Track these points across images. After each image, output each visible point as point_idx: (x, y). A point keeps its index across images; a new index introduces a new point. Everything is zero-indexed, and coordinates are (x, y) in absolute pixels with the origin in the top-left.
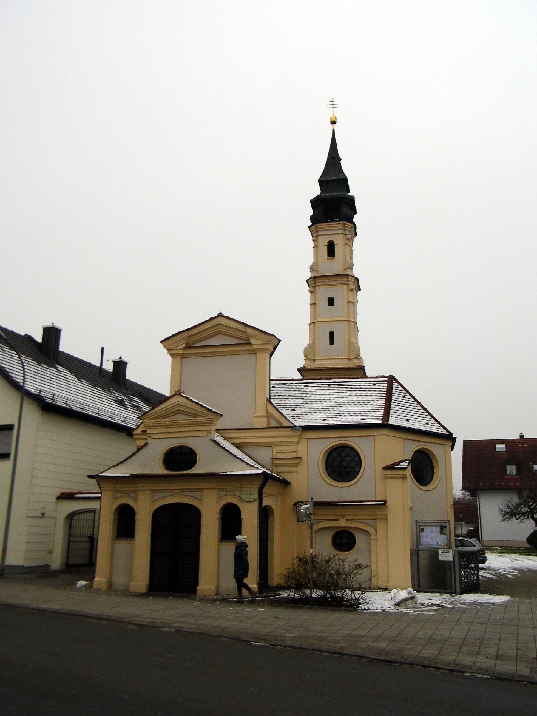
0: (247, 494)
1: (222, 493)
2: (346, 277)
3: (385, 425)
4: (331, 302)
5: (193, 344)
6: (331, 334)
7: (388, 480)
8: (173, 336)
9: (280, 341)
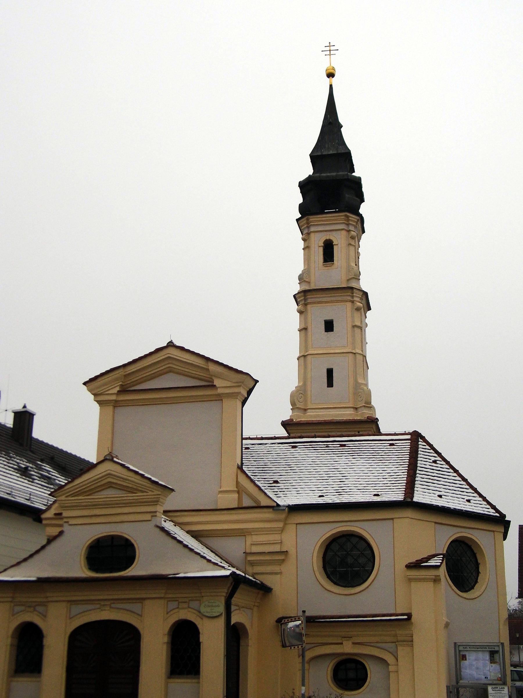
0: (209, 606)
1: (173, 605)
2: (350, 291)
4: (329, 326)
5: (131, 387)
6: (330, 373)
7: (413, 584)
8: (102, 375)
9: (257, 381)
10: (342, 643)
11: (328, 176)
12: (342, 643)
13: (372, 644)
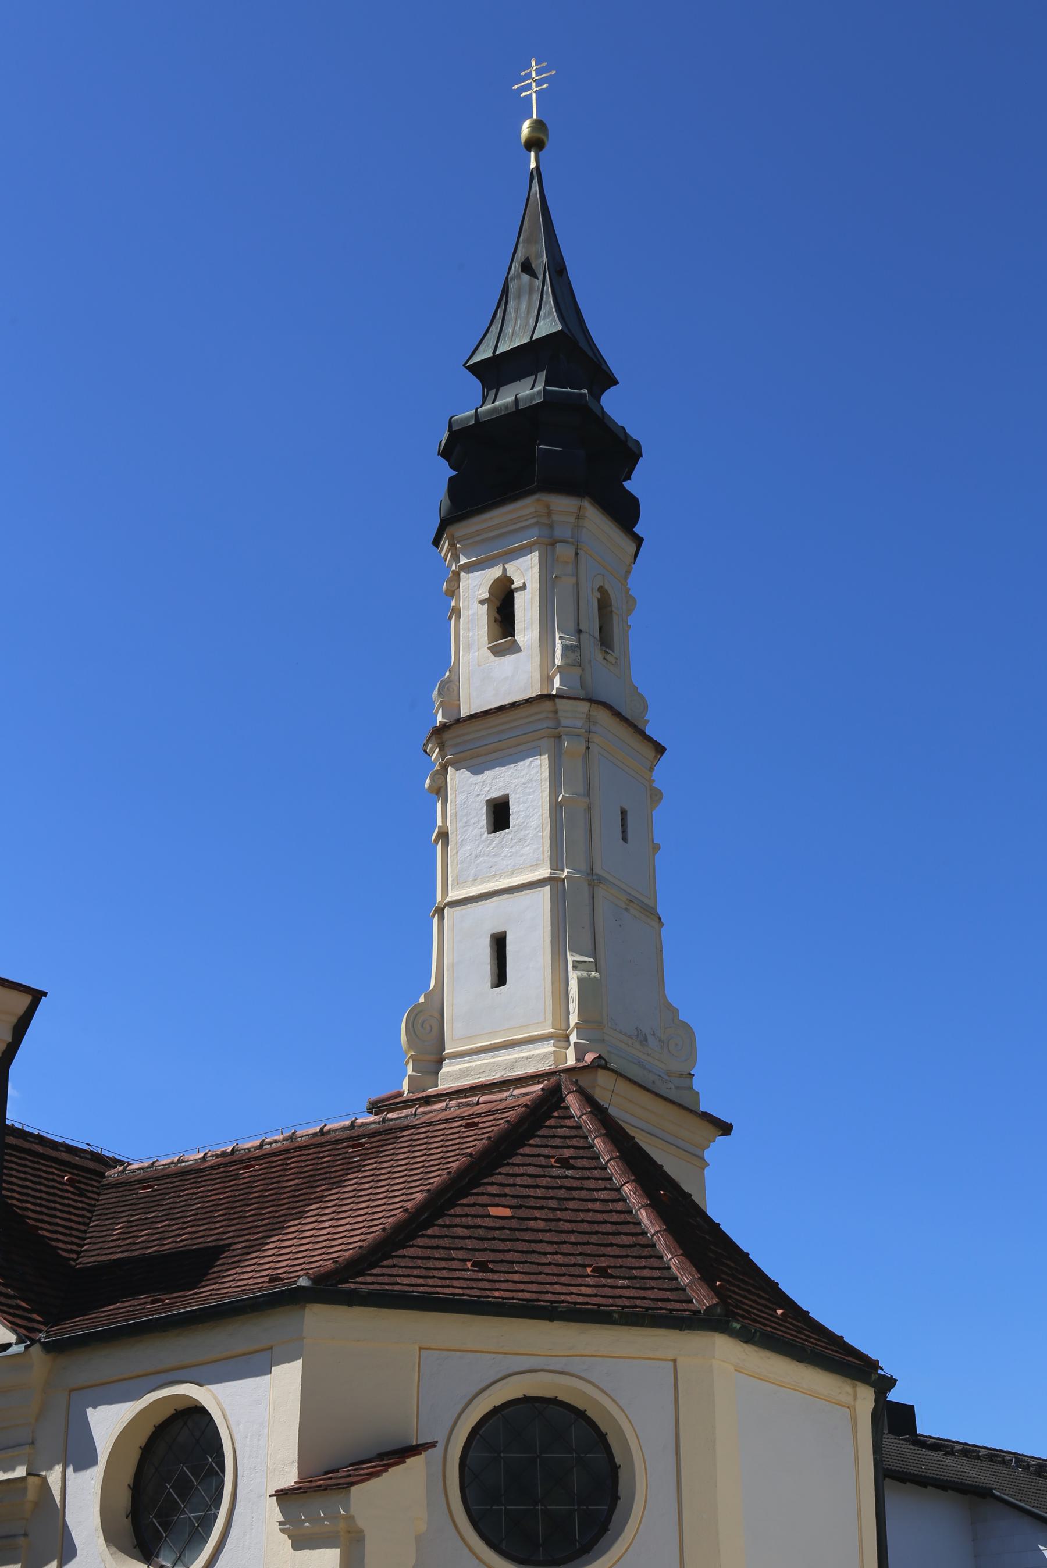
4: (499, 815)
6: (499, 943)
9: (37, 996)
11: (495, 410)
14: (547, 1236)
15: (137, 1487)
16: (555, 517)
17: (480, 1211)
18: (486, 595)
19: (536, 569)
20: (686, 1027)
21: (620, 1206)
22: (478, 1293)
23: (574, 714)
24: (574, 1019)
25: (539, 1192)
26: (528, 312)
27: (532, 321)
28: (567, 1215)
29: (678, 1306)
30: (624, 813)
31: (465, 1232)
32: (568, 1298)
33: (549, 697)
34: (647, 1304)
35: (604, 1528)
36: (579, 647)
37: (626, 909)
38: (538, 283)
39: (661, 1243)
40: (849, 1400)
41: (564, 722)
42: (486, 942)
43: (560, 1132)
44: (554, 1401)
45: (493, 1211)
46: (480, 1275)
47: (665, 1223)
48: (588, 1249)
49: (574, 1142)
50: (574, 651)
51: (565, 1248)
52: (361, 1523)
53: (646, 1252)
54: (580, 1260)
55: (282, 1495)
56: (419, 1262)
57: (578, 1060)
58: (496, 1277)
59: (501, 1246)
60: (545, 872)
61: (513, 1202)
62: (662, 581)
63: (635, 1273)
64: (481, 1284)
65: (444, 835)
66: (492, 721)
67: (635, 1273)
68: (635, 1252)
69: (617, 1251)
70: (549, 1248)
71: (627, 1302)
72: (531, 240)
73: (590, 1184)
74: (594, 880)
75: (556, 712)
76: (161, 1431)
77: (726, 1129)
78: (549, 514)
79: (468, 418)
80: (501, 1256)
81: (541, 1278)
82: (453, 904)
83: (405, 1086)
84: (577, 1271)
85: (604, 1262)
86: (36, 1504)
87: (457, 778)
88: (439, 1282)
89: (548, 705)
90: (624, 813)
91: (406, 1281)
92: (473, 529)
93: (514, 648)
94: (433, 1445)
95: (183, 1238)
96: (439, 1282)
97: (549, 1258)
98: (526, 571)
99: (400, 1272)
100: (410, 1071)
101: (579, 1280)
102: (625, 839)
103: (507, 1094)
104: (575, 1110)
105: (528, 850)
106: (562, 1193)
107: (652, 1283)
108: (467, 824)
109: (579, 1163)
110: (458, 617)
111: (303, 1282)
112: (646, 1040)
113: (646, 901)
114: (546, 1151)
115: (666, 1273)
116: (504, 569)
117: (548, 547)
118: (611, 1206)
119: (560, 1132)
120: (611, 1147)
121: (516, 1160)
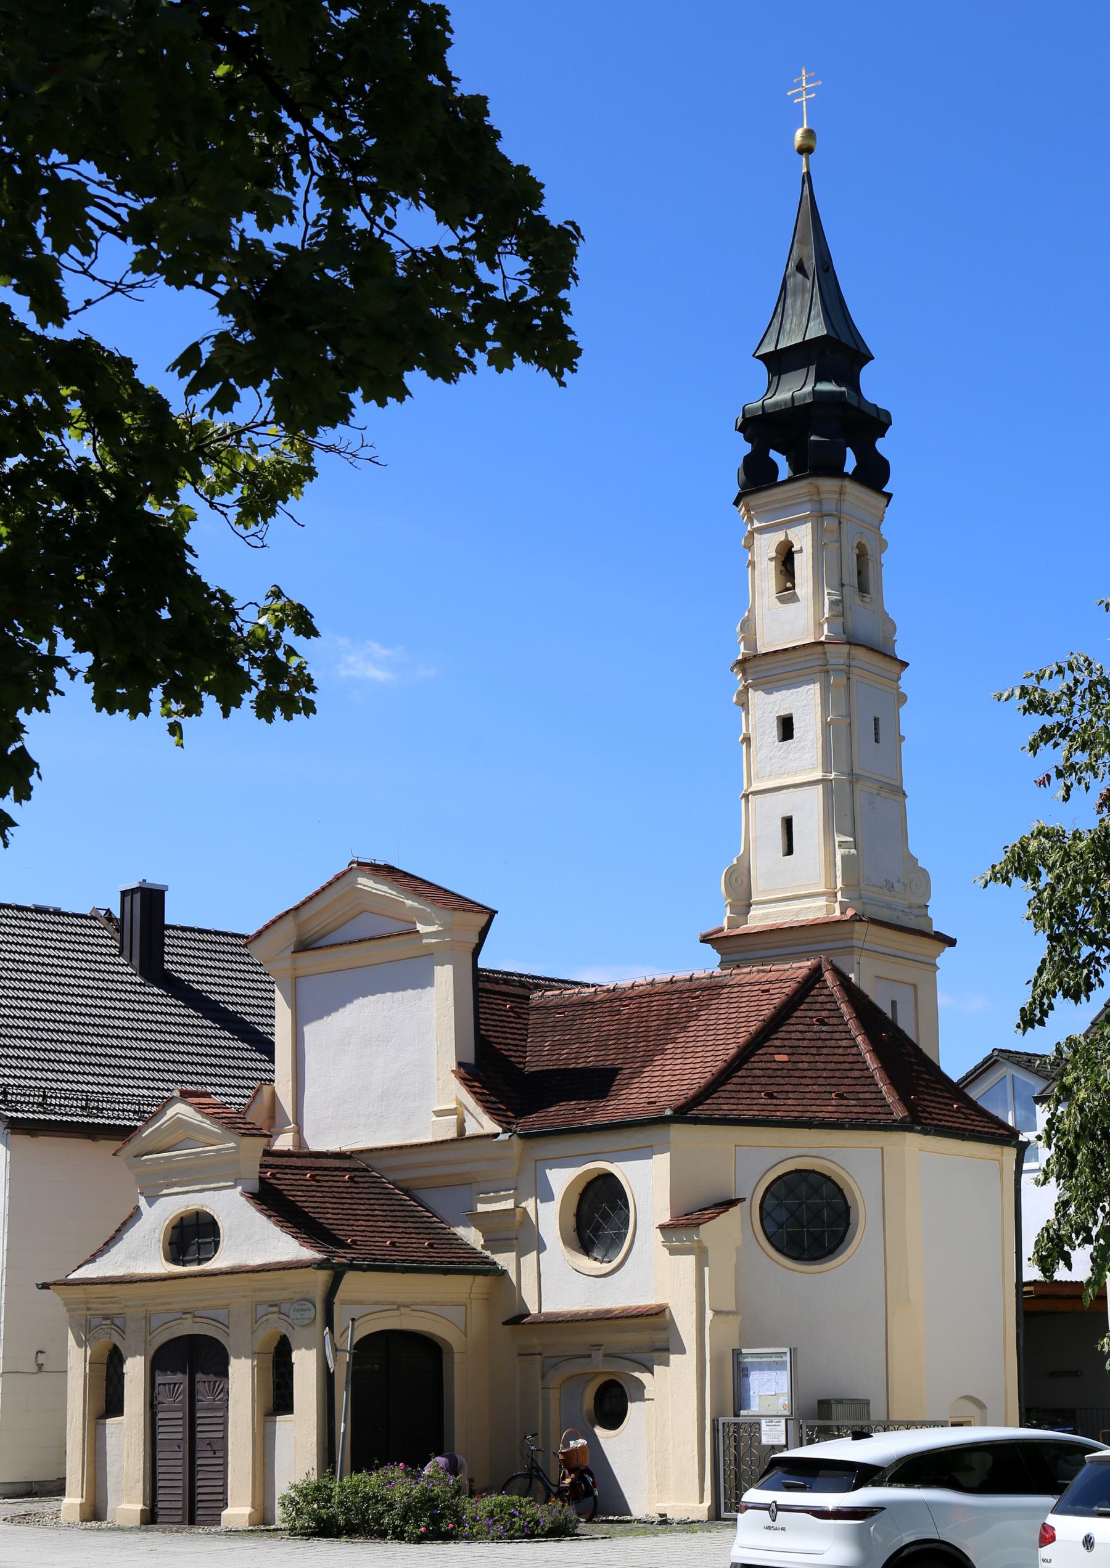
0: (298, 1310)
3: (461, 1137)
4: (786, 728)
6: (788, 823)
10: (590, 1356)
11: (777, 404)
12: (590, 1356)
13: (628, 1356)
14: (809, 1073)
15: (579, 1215)
16: (823, 496)
17: (769, 1058)
18: (774, 554)
19: (810, 537)
20: (924, 871)
21: (854, 1051)
22: (767, 1113)
23: (838, 654)
24: (839, 885)
25: (805, 1043)
26: (802, 312)
27: (807, 325)
28: (822, 1058)
29: (884, 1117)
30: (876, 720)
31: (760, 1073)
32: (820, 1115)
33: (822, 643)
34: (867, 1116)
35: (842, 1240)
36: (842, 601)
37: (878, 794)
38: (809, 284)
39: (877, 1076)
40: (998, 1156)
41: (831, 661)
42: (779, 822)
43: (820, 999)
44: (813, 1171)
45: (778, 1058)
46: (770, 1101)
47: (881, 1062)
48: (833, 1081)
49: (828, 1006)
50: (838, 605)
51: (820, 1081)
52: (706, 1243)
53: (868, 1081)
54: (828, 1088)
55: (663, 1228)
56: (734, 1094)
57: (842, 913)
58: (778, 1102)
59: (782, 1081)
60: (818, 775)
61: (789, 1051)
62: (910, 524)
63: (861, 1096)
64: (769, 1107)
65: (747, 740)
66: (779, 657)
67: (861, 1096)
68: (861, 1081)
69: (851, 1081)
70: (810, 1081)
71: (854, 1116)
72: (803, 242)
73: (837, 1036)
74: (853, 778)
75: (825, 653)
76: (590, 1185)
77: (952, 942)
78: (819, 493)
79: (756, 409)
80: (781, 1088)
81: (805, 1102)
82: (755, 793)
83: (725, 924)
84: (826, 1096)
85: (843, 1089)
86: (521, 1223)
87: (756, 697)
88: (745, 1107)
89: (819, 649)
90: (876, 720)
91: (726, 1107)
92: (761, 501)
93: (794, 599)
94: (744, 1200)
95: (591, 1059)
96: (745, 1107)
97: (810, 1088)
98: (802, 537)
99: (723, 1101)
100: (728, 914)
101: (827, 1102)
102: (877, 741)
103: (787, 966)
104: (829, 983)
105: (806, 757)
106: (819, 1043)
107: (871, 1102)
108: (763, 733)
109: (831, 1021)
110: (754, 568)
111: (668, 1112)
112: (893, 887)
113: (894, 783)
114: (810, 1014)
115: (879, 1096)
116: (787, 534)
117: (819, 517)
118: (849, 1051)
119: (820, 999)
120: (850, 1010)
121: (791, 1021)
